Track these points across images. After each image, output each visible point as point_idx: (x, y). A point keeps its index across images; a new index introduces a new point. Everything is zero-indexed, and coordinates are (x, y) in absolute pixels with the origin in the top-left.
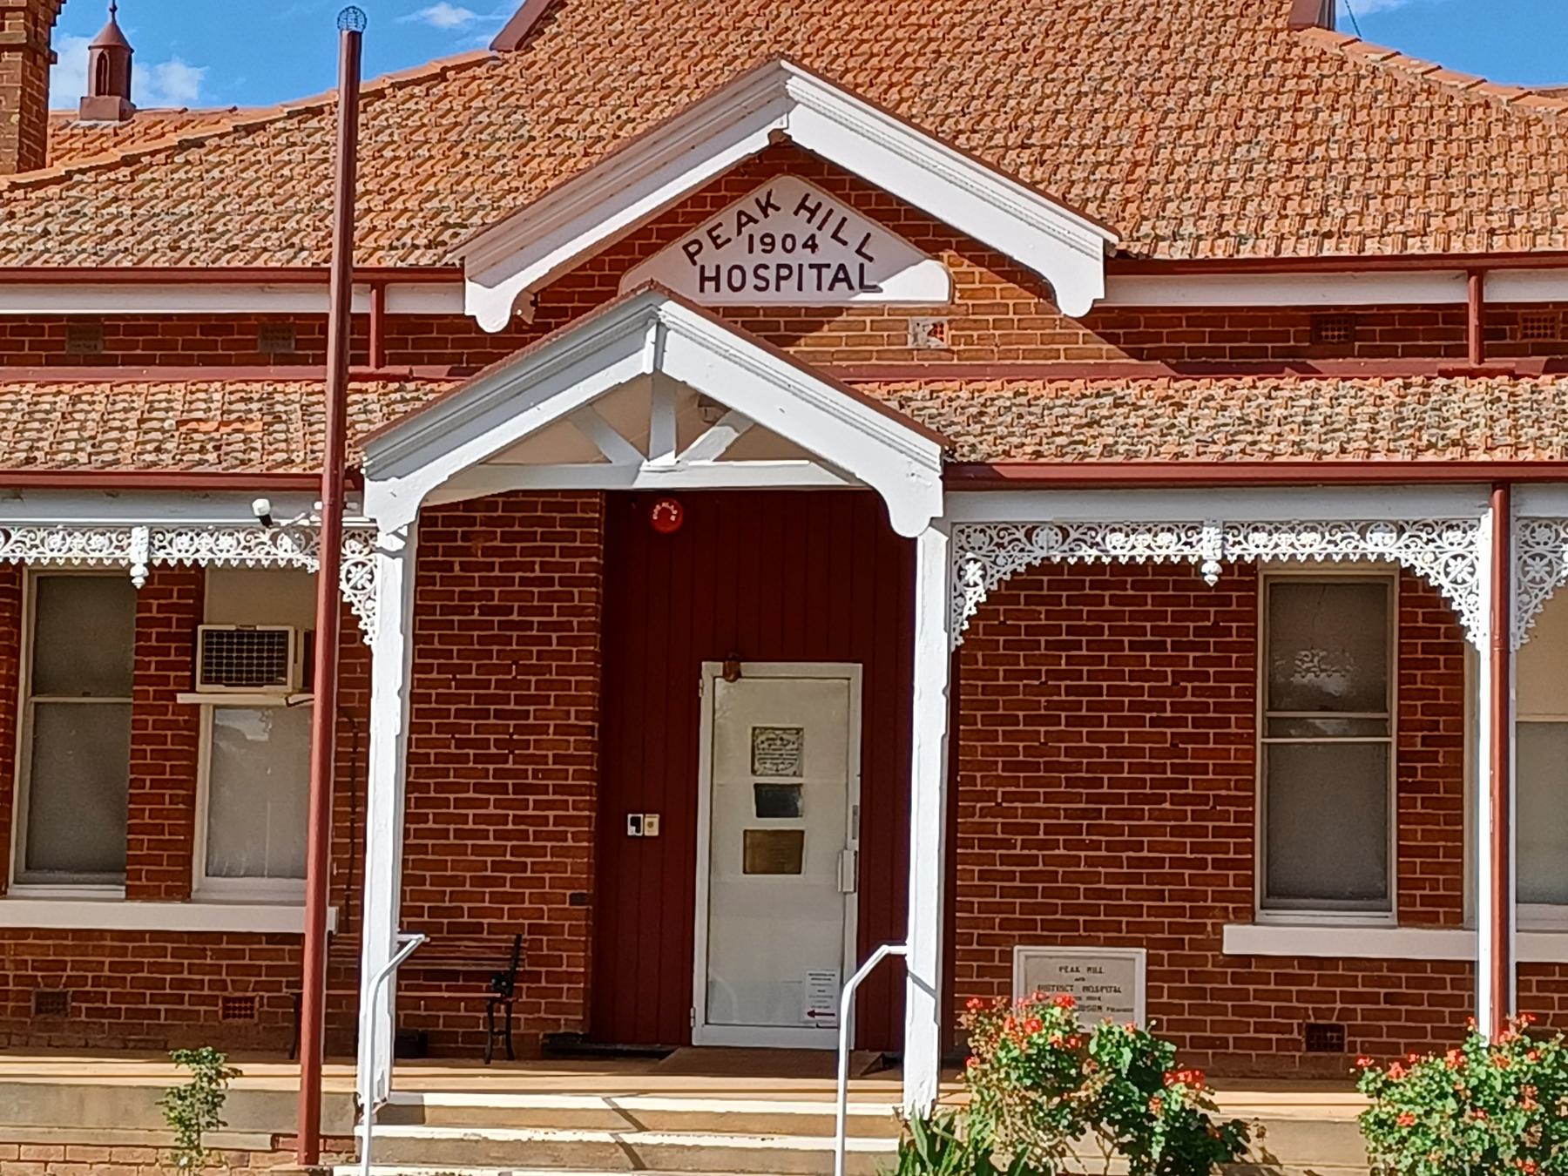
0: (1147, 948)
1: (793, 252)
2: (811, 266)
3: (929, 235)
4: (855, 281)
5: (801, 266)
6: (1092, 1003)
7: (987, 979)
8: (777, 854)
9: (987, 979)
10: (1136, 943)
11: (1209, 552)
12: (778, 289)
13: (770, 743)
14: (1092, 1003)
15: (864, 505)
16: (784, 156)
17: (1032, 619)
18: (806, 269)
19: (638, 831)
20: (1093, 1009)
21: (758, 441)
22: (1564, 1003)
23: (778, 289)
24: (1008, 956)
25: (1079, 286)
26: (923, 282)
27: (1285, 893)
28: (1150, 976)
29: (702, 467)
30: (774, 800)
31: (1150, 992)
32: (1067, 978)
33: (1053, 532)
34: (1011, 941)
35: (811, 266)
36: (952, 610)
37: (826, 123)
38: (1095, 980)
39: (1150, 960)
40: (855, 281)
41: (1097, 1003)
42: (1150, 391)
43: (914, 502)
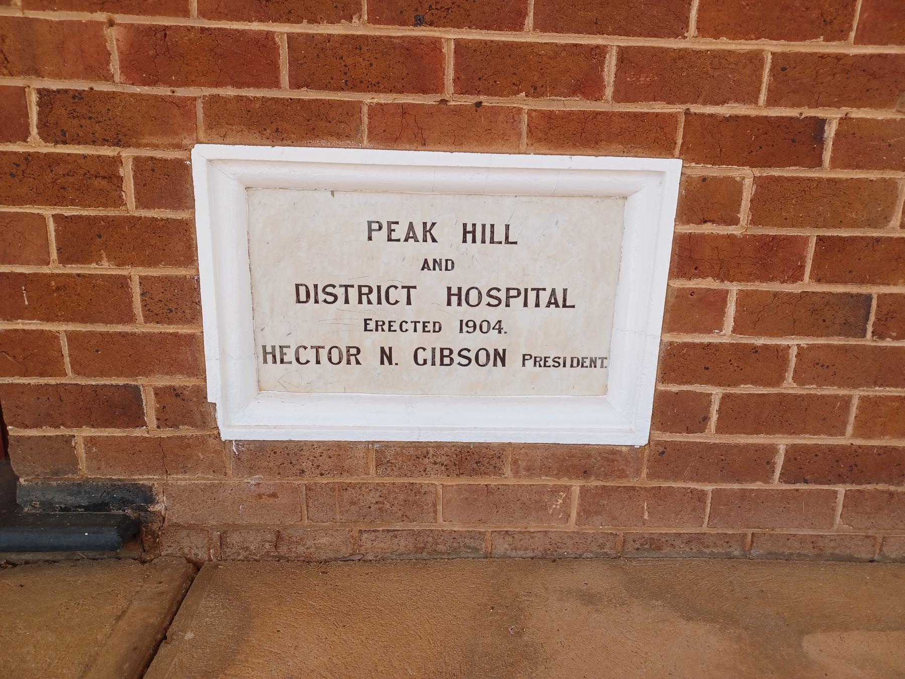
0: (689, 154)
2: (532, 289)
4: (560, 303)
5: (526, 290)
6: (474, 341)
7: (105, 268)
9: (105, 268)
10: (647, 138)
12: (508, 305)
14: (474, 341)
18: (529, 290)
20: (468, 358)
23: (508, 305)
24: (171, 183)
28: (687, 257)
31: (681, 311)
32: (395, 263)
34: (175, 121)
35: (532, 289)
38: (482, 268)
39: (696, 203)
40: (560, 303)
41: (493, 341)
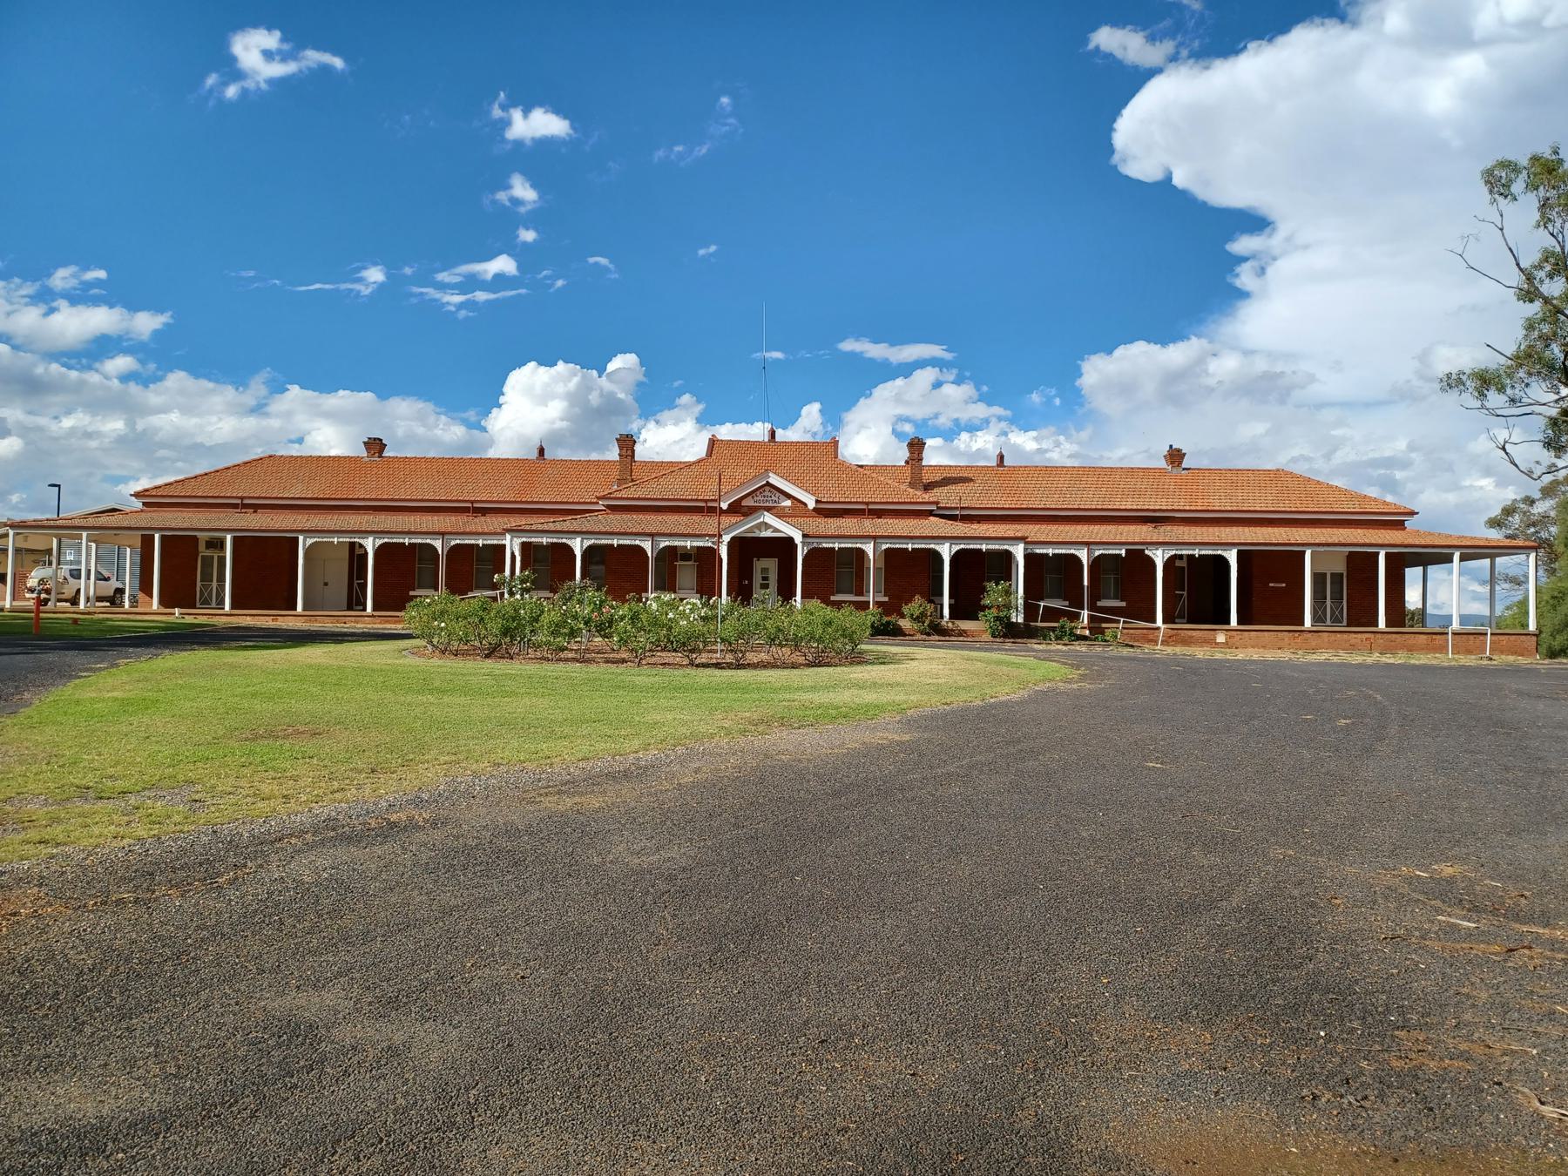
1: (770, 499)
3: (789, 496)
8: (764, 586)
11: (836, 546)
13: (765, 570)
15: (791, 539)
16: (768, 484)
17: (813, 556)
19: (367, 286)
21: (776, 530)
22: (1566, 962)
25: (811, 505)
26: (788, 503)
27: (839, 592)
29: (768, 534)
30: (765, 578)
33: (815, 543)
36: (750, 530)
37: (774, 480)
42: (822, 520)
43: (798, 539)
